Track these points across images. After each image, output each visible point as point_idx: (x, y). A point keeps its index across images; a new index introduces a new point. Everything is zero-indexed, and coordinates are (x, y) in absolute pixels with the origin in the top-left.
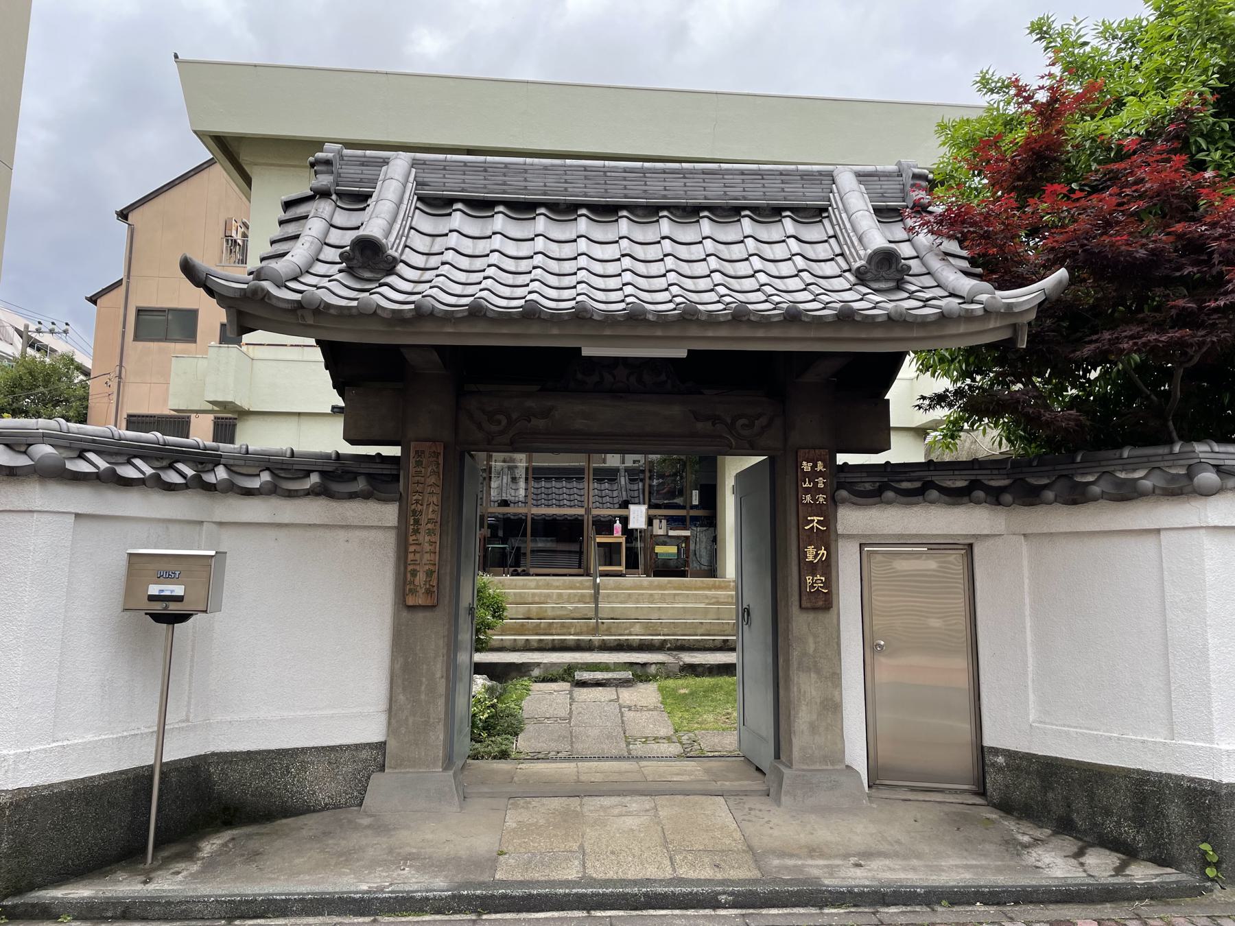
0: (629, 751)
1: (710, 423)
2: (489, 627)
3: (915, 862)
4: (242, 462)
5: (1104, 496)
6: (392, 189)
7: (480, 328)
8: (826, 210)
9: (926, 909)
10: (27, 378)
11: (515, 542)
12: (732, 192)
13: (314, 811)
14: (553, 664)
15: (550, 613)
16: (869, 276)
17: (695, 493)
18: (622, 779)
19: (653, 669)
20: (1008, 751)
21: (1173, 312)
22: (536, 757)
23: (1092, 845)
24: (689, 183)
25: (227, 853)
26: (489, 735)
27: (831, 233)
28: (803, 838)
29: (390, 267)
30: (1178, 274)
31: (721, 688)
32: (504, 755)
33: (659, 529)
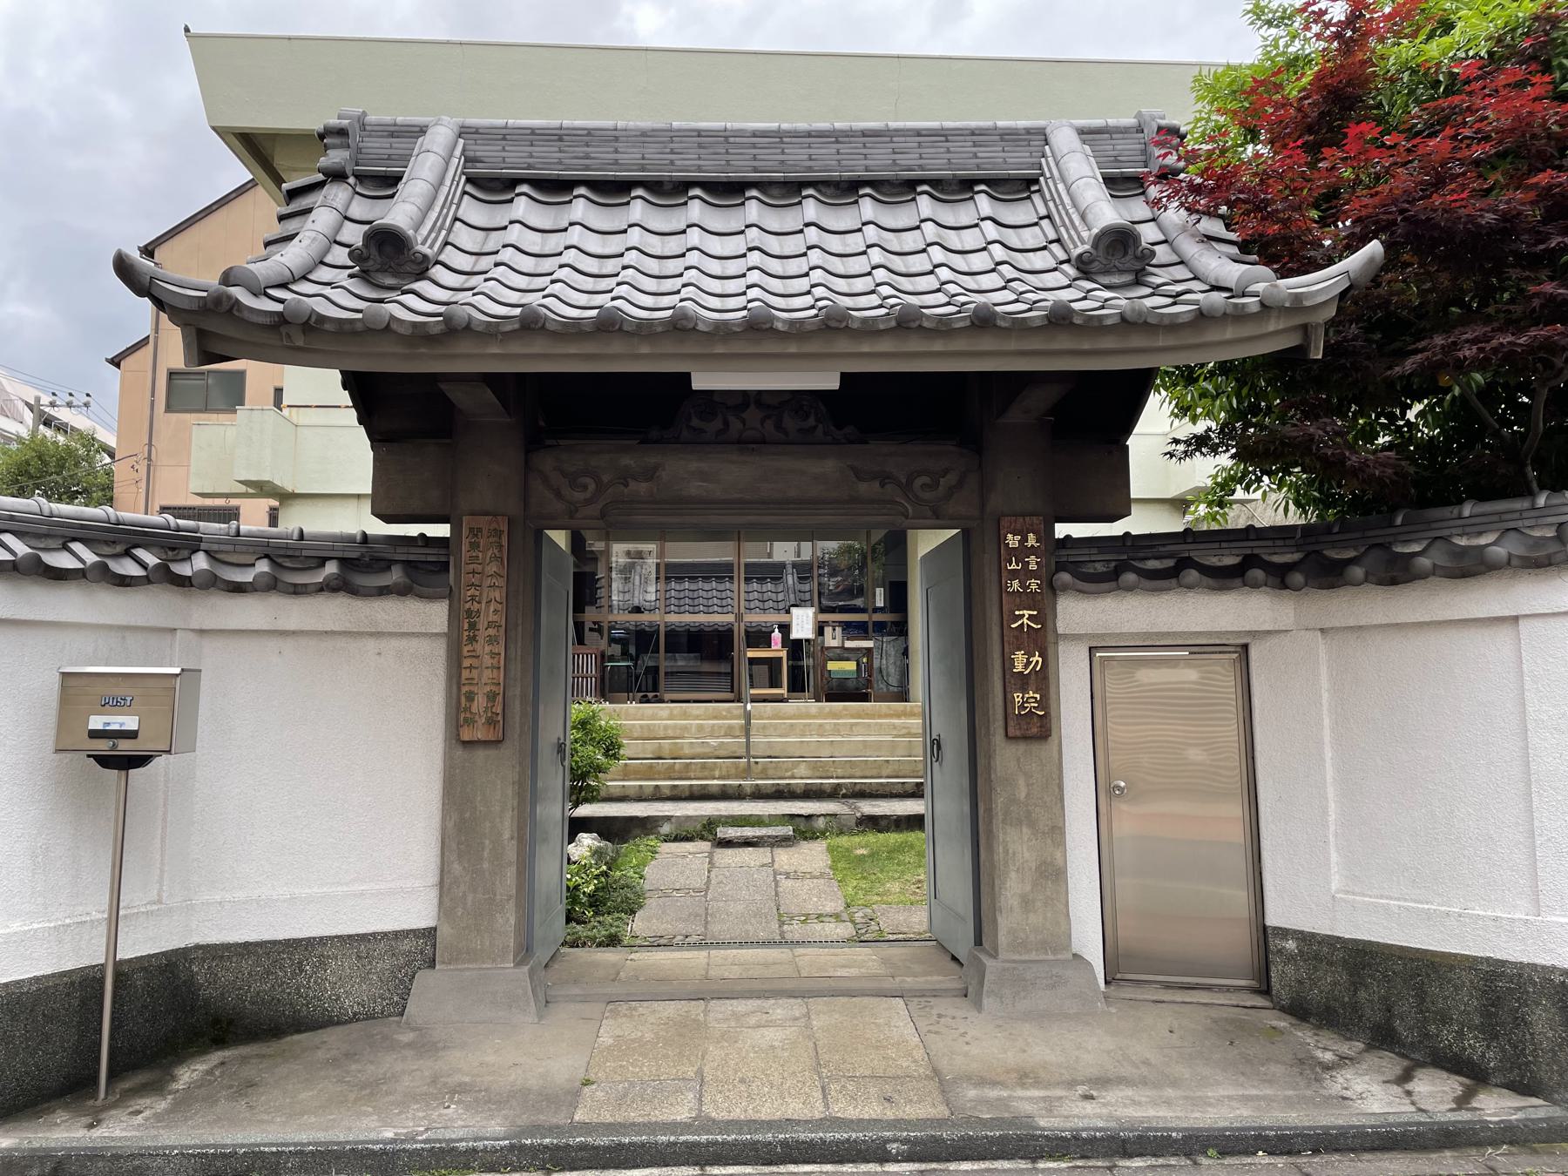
0: (782, 934)
1: (877, 484)
2: (599, 769)
3: (1170, 1092)
4: (230, 548)
5: (1436, 571)
6: (428, 164)
7: (538, 346)
8: (1036, 181)
9: (1184, 1161)
10: (36, 463)
11: (647, 661)
12: (904, 160)
13: (339, 1023)
14: (688, 818)
15: (687, 751)
16: (1095, 266)
17: (880, 592)
18: (768, 973)
19: (821, 823)
20: (1302, 932)
21: (1536, 302)
22: (657, 944)
23: (1423, 1065)
24: (844, 149)
25: (211, 1083)
26: (596, 914)
27: (1043, 212)
28: (1012, 1058)
29: (421, 268)
30: (1542, 247)
31: (912, 847)
32: (613, 941)
33: (832, 639)
